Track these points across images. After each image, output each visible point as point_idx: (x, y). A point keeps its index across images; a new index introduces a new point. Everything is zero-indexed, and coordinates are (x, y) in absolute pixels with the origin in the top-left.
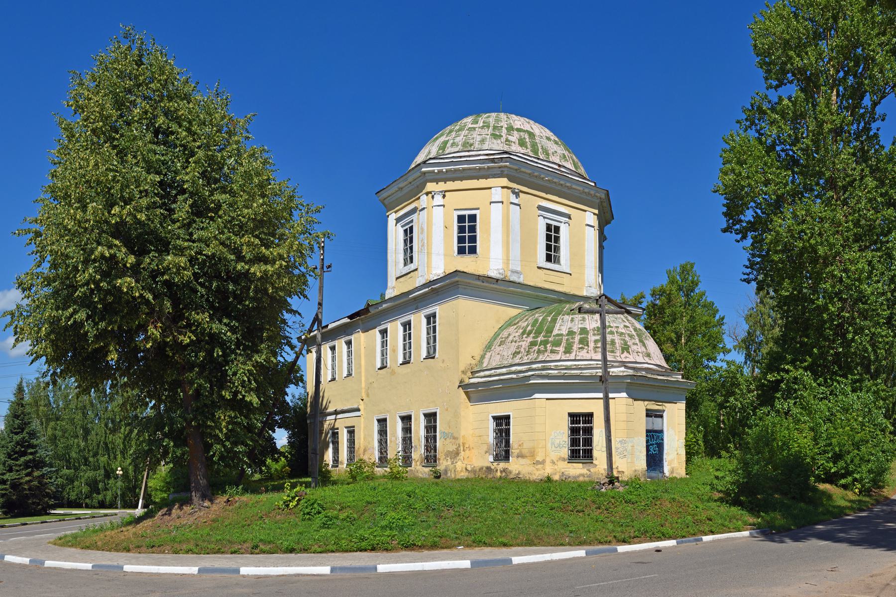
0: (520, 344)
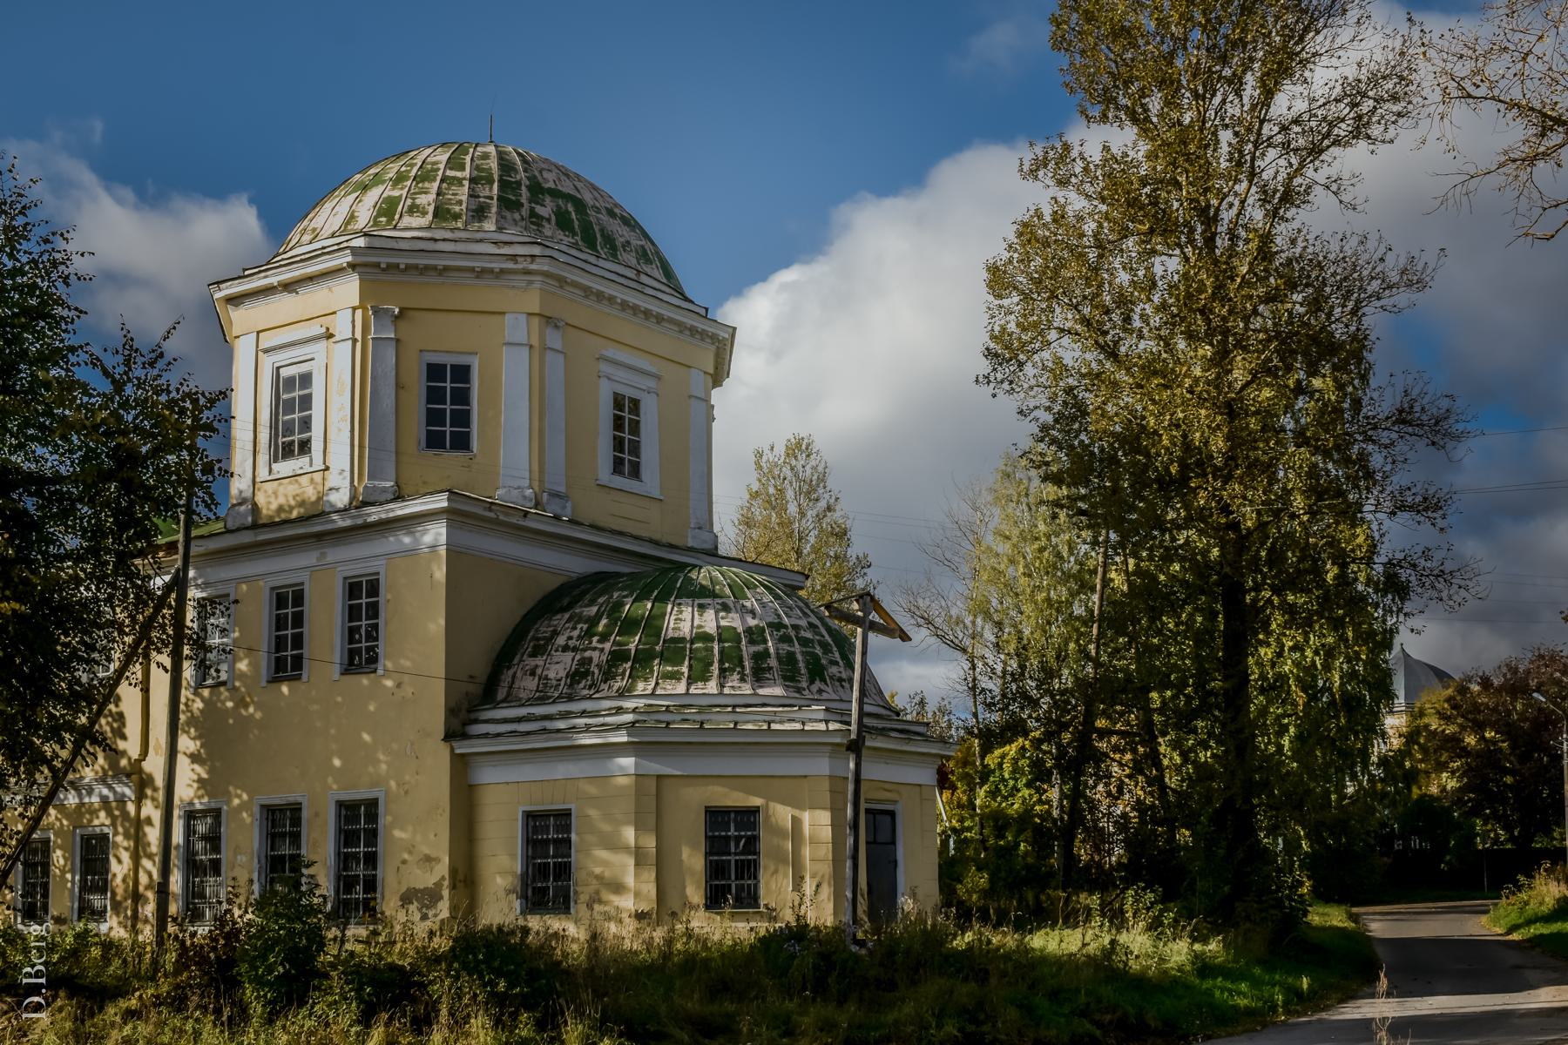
0: (587, 654)
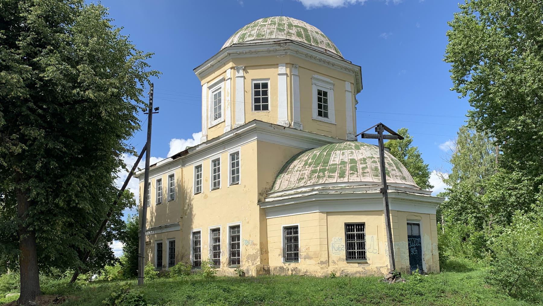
0: (304, 172)
